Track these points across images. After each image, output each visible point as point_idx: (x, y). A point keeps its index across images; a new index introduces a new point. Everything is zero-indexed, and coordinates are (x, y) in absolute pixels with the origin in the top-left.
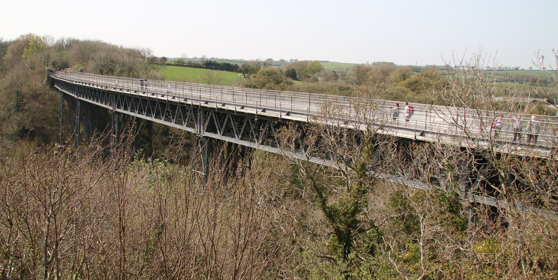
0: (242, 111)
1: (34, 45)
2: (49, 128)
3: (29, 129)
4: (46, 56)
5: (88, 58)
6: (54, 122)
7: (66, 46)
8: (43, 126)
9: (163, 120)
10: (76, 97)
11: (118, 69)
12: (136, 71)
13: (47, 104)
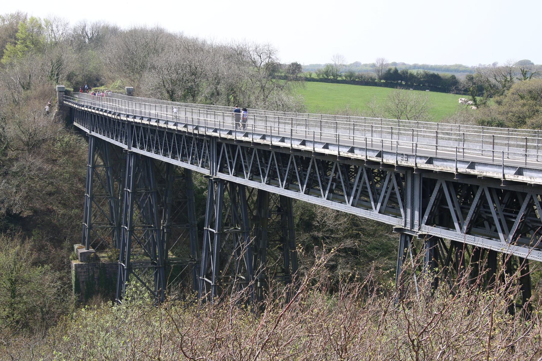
0: (520, 179)
1: (27, 36)
2: (62, 211)
3: (20, 213)
4: (54, 61)
5: (143, 67)
6: (72, 199)
7: (90, 39)
8: (50, 207)
9: (349, 205)
10: (126, 147)
11: (206, 89)
12: (243, 93)
13: (59, 162)
